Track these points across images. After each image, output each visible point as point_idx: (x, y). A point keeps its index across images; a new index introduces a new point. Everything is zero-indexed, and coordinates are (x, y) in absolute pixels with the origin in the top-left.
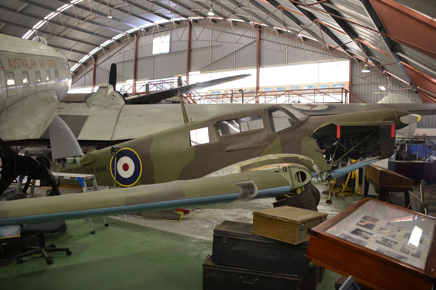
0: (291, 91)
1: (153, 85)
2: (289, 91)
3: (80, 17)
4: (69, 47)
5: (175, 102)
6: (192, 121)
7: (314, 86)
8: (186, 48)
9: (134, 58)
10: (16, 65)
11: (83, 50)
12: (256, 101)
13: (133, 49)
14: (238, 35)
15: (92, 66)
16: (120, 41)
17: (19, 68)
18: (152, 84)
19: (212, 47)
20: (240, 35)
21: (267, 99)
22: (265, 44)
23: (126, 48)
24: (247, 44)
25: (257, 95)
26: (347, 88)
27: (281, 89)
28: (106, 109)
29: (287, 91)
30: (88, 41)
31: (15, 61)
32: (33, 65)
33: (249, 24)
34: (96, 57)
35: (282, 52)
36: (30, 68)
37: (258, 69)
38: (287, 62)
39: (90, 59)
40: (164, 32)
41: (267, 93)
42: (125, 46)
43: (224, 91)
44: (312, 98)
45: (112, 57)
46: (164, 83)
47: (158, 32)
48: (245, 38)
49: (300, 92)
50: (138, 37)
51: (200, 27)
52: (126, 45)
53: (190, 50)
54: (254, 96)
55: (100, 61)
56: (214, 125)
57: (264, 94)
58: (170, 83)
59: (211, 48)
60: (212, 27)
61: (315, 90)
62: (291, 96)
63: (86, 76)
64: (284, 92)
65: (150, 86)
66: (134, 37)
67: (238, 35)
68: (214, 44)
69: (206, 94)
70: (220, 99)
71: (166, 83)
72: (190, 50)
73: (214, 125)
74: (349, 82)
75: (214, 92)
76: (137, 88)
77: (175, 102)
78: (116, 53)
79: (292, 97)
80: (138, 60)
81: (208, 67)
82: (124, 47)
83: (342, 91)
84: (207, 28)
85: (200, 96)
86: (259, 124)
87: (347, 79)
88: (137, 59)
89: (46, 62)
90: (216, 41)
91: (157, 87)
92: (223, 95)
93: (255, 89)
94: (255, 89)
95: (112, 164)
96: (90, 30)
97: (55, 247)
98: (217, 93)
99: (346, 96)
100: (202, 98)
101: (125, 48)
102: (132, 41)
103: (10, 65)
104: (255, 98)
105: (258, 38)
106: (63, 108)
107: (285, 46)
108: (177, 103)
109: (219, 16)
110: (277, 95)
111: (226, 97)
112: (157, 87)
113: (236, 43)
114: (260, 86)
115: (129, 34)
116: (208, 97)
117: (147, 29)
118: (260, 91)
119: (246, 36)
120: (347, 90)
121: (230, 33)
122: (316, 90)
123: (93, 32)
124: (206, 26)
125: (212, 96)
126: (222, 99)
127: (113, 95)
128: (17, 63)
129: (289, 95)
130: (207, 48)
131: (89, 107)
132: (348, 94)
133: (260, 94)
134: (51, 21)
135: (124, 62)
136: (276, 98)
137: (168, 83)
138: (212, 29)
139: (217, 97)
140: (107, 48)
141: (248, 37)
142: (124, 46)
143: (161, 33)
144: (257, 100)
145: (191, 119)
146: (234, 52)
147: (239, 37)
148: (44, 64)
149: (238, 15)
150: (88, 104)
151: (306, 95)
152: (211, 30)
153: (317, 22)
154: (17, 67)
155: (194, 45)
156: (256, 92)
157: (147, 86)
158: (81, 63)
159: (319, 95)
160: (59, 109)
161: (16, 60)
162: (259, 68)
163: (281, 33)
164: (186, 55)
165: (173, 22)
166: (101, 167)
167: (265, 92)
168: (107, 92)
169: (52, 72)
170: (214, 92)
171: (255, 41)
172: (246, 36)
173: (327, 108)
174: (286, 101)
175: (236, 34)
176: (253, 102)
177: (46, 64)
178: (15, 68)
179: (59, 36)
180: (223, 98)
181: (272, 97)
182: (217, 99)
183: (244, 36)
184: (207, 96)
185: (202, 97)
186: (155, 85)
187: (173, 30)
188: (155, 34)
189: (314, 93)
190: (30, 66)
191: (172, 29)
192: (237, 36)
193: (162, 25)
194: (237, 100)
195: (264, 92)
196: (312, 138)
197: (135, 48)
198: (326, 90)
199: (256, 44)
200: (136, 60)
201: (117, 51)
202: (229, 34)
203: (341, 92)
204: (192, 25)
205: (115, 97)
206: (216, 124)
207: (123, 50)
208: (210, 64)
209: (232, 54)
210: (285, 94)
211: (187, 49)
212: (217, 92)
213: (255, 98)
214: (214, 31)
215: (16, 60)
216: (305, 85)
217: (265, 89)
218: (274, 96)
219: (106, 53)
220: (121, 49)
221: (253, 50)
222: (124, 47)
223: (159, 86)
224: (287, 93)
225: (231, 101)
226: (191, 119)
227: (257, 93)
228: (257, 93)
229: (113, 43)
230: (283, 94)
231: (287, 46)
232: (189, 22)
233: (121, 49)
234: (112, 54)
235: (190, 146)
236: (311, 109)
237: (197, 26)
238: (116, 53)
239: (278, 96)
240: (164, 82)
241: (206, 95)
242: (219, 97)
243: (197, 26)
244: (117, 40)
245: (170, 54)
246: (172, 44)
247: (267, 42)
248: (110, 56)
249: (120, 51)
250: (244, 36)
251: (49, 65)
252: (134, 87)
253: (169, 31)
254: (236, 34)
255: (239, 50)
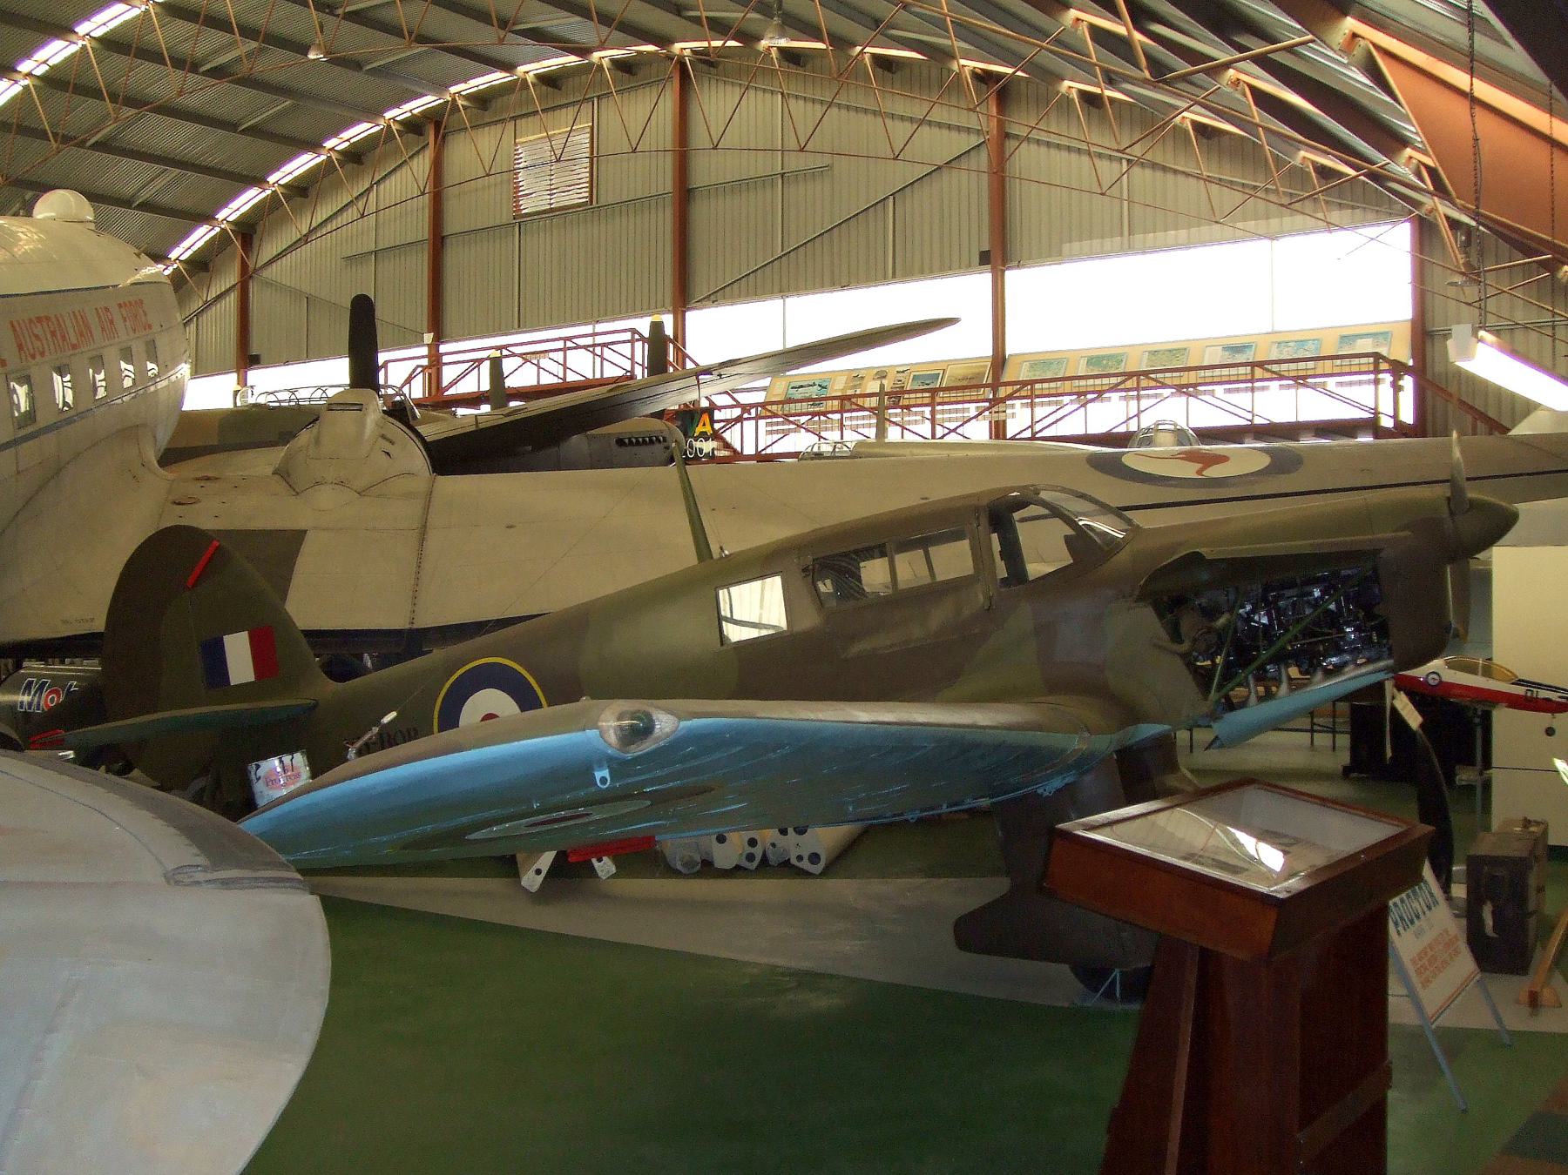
0: (1146, 374)
1: (519, 361)
2: (1138, 374)
3: (185, 61)
4: (128, 190)
5: (630, 439)
6: (727, 552)
7: (1256, 346)
8: (665, 181)
9: (426, 237)
10: (37, 344)
11: (187, 204)
12: (990, 422)
13: (423, 194)
14: (902, 118)
15: (231, 278)
16: (360, 156)
17: (42, 354)
18: (514, 355)
19: (785, 179)
20: (911, 120)
21: (1040, 412)
22: (1026, 158)
23: (388, 187)
24: (941, 164)
25: (994, 395)
26: (1404, 354)
27: (1105, 362)
28: (365, 498)
29: (1130, 375)
30: (213, 160)
31: (31, 329)
32: (82, 335)
33: (950, 71)
34: (247, 230)
35: (1103, 194)
36: (74, 347)
37: (999, 273)
38: (1126, 233)
39: (218, 245)
40: (564, 110)
41: (1037, 386)
42: (384, 178)
43: (845, 378)
44: (1243, 399)
45: (324, 231)
46: (569, 348)
47: (535, 113)
48: (936, 130)
49: (1192, 377)
50: (444, 137)
51: (729, 88)
52: (390, 173)
53: (684, 195)
54: (983, 401)
55: (268, 250)
56: (804, 570)
57: (1028, 390)
58: (591, 349)
59: (780, 181)
60: (781, 87)
61: (1253, 365)
62: (1148, 396)
63: (204, 318)
64: (1114, 380)
65: (508, 365)
66: (421, 135)
67: (902, 118)
68: (796, 162)
69: (764, 393)
70: (830, 416)
71: (578, 347)
72: (684, 195)
73: (804, 570)
74: (1413, 321)
75: (802, 386)
76: (448, 374)
77: (627, 441)
78: (341, 210)
79: (1154, 401)
80: (448, 241)
81: (768, 269)
82: (378, 183)
83: (1376, 364)
84: (760, 89)
85: (738, 405)
86: (953, 559)
87: (1403, 309)
88: (443, 238)
89: (115, 311)
90: (802, 150)
91: (539, 368)
92: (843, 398)
93: (987, 366)
94: (987, 366)
95: (441, 708)
96: (222, 110)
97: (1225, 389)
98: (814, 392)
99: (1397, 389)
100: (746, 415)
101: (382, 186)
102: (418, 153)
103: (20, 347)
104: (988, 409)
105: (995, 132)
106: (193, 501)
107: (1115, 165)
108: (638, 443)
109: (811, 38)
110: (1085, 394)
111: (854, 407)
112: (539, 368)
113: (896, 158)
114: (1011, 348)
115: (402, 123)
116: (774, 408)
117: (482, 100)
118: (1006, 378)
119: (940, 125)
120: (1403, 360)
121: (866, 111)
122: (1261, 364)
123: (235, 120)
124: (754, 79)
125: (792, 405)
126: (837, 416)
127: (383, 437)
128: (37, 337)
129: (1137, 389)
130: (766, 180)
131: (298, 493)
132: (1408, 382)
133: (1010, 390)
134: (54, 81)
135: (379, 255)
136: (1084, 405)
137: (585, 347)
138: (782, 94)
139: (817, 409)
140: (301, 190)
141: (949, 127)
142: (377, 178)
143: (550, 114)
144: (995, 417)
145: (721, 548)
146: (887, 197)
147: (908, 128)
148: (112, 322)
149: (897, 36)
150: (289, 476)
151: (1219, 389)
152: (780, 96)
153: (1238, 80)
154: (37, 354)
155: (705, 170)
156: (990, 381)
157: (496, 365)
158: (180, 261)
159: (1276, 384)
160: (179, 504)
161: (32, 325)
162: (1003, 272)
163: (1097, 108)
164: (665, 220)
165: (602, 65)
166: (400, 731)
167: (1032, 382)
168: (363, 424)
169: (138, 348)
170: (802, 386)
171: (978, 146)
172: (940, 125)
173: (1268, 464)
174: (1372, 239)
175: (893, 116)
176: (979, 431)
177: (119, 324)
178: (33, 357)
179: (81, 144)
180: (841, 411)
181: (1066, 399)
182: (816, 418)
183: (930, 123)
184: (769, 407)
185: (746, 408)
186: (528, 357)
187: (604, 101)
188: (522, 123)
189: (1252, 381)
190: (75, 342)
191: (598, 97)
192: (898, 123)
193: (549, 81)
194: (906, 419)
195: (1024, 384)
196: (1141, 604)
197: (432, 190)
198: (1302, 365)
199: (982, 159)
200: (438, 242)
201: (345, 202)
202: (861, 115)
203: (1372, 368)
204: (690, 78)
205: (392, 443)
206: (811, 567)
207: (373, 195)
208: (781, 257)
209: (880, 206)
210: (1122, 386)
211: (669, 188)
212: (814, 385)
213: (988, 409)
214: (792, 102)
215: (32, 325)
216: (1208, 343)
217: (1031, 367)
218: (1075, 397)
219: (297, 211)
220: (369, 190)
221: (971, 186)
222: (378, 183)
223: (545, 363)
224: (1131, 383)
225: (881, 432)
226: (721, 548)
227: (994, 387)
228: (994, 387)
229: (327, 167)
230: (1114, 388)
231: (1125, 163)
232: (675, 65)
233: (369, 190)
234: (324, 217)
235: (719, 645)
236: (1199, 472)
237: (713, 82)
238: (341, 210)
239: (1090, 396)
240: (569, 344)
241: (761, 400)
242: (822, 409)
243: (713, 82)
244: (343, 153)
245: (596, 214)
246: (603, 168)
247: (1033, 147)
248: (314, 225)
249: (361, 204)
250: (930, 123)
251: (127, 323)
252: (434, 369)
253: (586, 107)
254: (893, 116)
255: (908, 190)
